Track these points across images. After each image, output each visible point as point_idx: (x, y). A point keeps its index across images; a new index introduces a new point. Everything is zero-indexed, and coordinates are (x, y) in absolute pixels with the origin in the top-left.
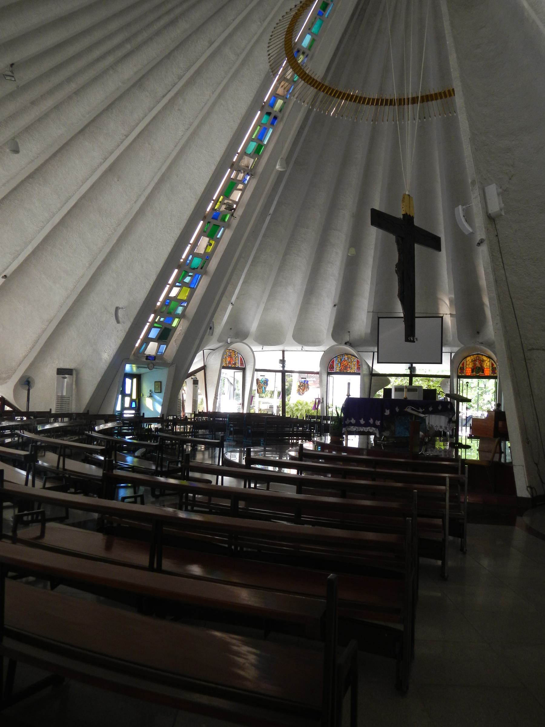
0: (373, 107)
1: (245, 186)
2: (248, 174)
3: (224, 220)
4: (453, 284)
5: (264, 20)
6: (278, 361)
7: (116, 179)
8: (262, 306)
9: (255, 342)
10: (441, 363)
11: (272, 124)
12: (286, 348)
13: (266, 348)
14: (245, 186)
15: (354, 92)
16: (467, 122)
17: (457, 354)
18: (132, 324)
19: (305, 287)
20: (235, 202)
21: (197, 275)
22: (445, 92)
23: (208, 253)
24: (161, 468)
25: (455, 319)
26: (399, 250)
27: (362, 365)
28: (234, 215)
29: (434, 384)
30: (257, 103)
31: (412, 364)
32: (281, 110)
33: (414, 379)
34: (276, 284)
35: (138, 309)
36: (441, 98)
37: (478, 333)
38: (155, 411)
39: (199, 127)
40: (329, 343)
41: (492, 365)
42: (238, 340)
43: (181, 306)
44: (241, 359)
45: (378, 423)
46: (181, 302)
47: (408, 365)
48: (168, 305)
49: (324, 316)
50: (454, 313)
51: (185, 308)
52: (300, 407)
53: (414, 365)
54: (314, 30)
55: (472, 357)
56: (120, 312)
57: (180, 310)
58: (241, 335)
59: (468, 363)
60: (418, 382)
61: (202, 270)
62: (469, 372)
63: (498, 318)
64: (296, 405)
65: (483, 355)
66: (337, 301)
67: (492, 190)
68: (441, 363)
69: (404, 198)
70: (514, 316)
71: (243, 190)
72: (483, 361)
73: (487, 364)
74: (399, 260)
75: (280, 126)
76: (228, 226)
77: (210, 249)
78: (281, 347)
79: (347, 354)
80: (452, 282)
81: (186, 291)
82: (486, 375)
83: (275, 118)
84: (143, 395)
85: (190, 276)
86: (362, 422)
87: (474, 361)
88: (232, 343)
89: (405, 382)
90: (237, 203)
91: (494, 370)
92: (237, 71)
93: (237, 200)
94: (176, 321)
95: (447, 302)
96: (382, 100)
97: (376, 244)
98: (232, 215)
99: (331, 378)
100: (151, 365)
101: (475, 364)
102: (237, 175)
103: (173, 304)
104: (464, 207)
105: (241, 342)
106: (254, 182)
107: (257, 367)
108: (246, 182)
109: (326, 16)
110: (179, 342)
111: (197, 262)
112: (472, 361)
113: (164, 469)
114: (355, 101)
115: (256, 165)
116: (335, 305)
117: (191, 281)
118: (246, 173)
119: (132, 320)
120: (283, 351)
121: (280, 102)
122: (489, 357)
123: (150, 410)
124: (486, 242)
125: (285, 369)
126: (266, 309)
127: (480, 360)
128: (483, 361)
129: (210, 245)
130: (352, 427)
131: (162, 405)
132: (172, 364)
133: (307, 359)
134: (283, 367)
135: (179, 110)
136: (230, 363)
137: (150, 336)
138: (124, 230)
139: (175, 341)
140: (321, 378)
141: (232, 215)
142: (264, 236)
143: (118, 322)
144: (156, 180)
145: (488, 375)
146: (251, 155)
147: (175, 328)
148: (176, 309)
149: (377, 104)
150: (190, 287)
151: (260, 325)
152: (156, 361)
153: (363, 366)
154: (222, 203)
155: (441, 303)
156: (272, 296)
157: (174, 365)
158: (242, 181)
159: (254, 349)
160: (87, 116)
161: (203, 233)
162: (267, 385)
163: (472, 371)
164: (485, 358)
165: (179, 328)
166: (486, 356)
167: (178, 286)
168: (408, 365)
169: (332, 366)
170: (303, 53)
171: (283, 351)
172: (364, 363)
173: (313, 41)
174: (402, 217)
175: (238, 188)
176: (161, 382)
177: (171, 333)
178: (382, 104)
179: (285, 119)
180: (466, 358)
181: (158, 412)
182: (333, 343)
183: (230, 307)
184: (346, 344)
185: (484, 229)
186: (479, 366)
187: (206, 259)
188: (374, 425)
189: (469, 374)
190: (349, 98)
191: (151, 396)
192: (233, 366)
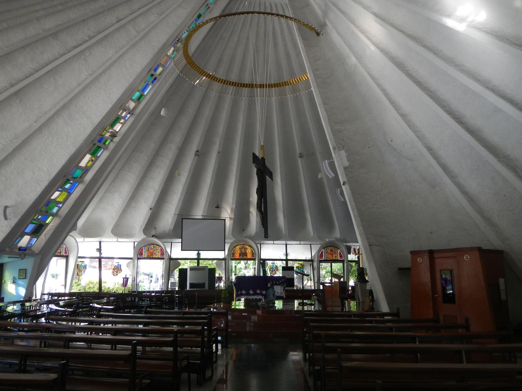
0: (221, 85)
3: (104, 144)
5: (161, 15)
6: (95, 250)
7: (18, 102)
9: (78, 235)
11: (153, 82)
12: (103, 240)
13: (87, 239)
14: (126, 121)
18: (19, 220)
19: (130, 195)
29: (212, 265)
32: (160, 75)
33: (200, 261)
35: (27, 208)
38: (18, 295)
39: (101, 74)
40: (140, 237)
41: (252, 251)
43: (57, 206)
44: (65, 249)
45: (264, 292)
49: (140, 215)
52: (92, 286)
53: (200, 252)
56: (8, 210)
57: (55, 210)
60: (203, 264)
63: (361, 227)
64: (88, 284)
66: (153, 206)
71: (123, 124)
72: (247, 249)
73: (249, 251)
75: (157, 84)
78: (98, 239)
79: (153, 244)
81: (65, 194)
83: (155, 79)
84: (5, 282)
85: (70, 183)
86: (251, 292)
87: (241, 249)
89: (194, 264)
91: (253, 254)
92: (137, 43)
93: (117, 130)
96: (228, 81)
97: (190, 170)
98: (112, 140)
99: (141, 261)
100: (23, 255)
101: (241, 251)
102: (122, 113)
103: (52, 204)
106: (132, 119)
107: (79, 255)
108: (127, 118)
110: (48, 236)
114: (219, 82)
115: (135, 108)
116: (151, 209)
119: (19, 217)
120: (100, 242)
121: (160, 69)
122: (250, 246)
123: (13, 295)
125: (102, 256)
128: (247, 249)
131: (26, 290)
133: (125, 248)
134: (101, 254)
137: (26, 231)
138: (21, 143)
139: (45, 235)
140: (134, 262)
141: (112, 140)
143: (6, 218)
144: (58, 108)
147: (48, 224)
149: (224, 83)
152: (27, 252)
158: (124, 118)
160: (6, 49)
162: (86, 268)
163: (240, 255)
164: (248, 247)
165: (50, 225)
167: (59, 191)
168: (197, 252)
169: (142, 253)
176: (26, 270)
178: (227, 84)
181: (21, 296)
182: (143, 236)
184: (153, 236)
188: (261, 294)
190: (208, 76)
191: (14, 282)
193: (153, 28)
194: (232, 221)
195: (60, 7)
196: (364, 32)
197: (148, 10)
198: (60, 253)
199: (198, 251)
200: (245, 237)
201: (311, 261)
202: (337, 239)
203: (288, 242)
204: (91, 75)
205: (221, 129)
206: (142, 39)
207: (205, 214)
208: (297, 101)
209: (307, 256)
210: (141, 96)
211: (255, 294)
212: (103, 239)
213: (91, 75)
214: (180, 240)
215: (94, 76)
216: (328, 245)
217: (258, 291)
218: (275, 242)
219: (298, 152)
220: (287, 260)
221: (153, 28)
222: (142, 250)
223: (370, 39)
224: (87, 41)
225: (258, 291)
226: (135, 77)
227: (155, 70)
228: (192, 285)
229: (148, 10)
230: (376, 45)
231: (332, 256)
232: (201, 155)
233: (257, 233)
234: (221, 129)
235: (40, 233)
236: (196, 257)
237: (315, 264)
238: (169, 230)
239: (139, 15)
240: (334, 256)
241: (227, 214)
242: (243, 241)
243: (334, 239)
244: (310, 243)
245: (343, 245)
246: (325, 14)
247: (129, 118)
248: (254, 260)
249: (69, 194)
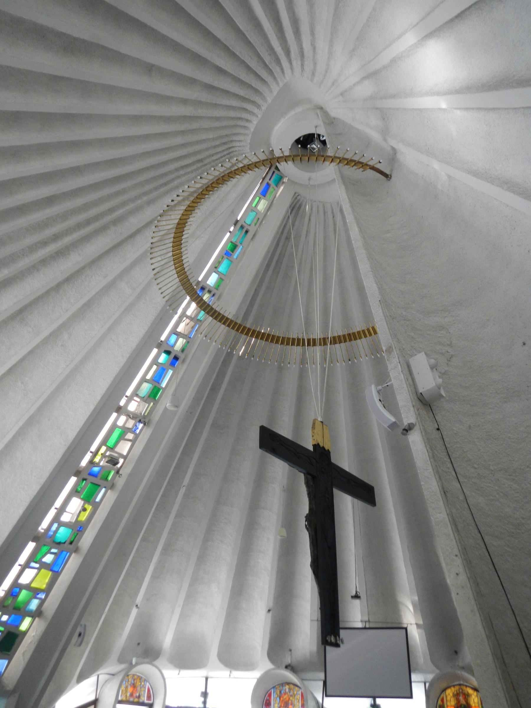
1: (137, 436)
2: (140, 421)
4: (414, 582)
6: (200, 694)
8: (178, 612)
10: (411, 697)
11: (172, 364)
14: (137, 436)
16: (375, 285)
17: (432, 684)
20: (122, 456)
21: (64, 553)
22: (368, 330)
23: (81, 521)
25: (422, 631)
26: (309, 494)
27: (307, 700)
28: (120, 472)
30: (151, 339)
31: (374, 698)
32: (183, 350)
34: (195, 580)
36: (366, 336)
37: (456, 652)
39: (82, 362)
40: (265, 666)
42: (146, 660)
43: (36, 598)
44: (149, 690)
46: (35, 592)
48: (16, 596)
49: (257, 627)
50: (421, 622)
51: (43, 602)
53: (379, 701)
54: (222, 268)
57: (34, 605)
58: (150, 653)
59: (449, 698)
61: (71, 546)
65: (466, 686)
66: (271, 605)
67: (420, 363)
68: (411, 697)
69: (314, 424)
70: (491, 567)
71: (133, 441)
74: (310, 509)
75: (181, 367)
76: (112, 486)
77: (84, 517)
78: (201, 673)
79: (288, 684)
80: (412, 577)
81: (46, 576)
83: (176, 358)
87: (456, 696)
88: (137, 664)
90: (125, 458)
94: (27, 621)
95: (411, 607)
101: (458, 701)
103: (23, 595)
104: (380, 387)
105: (150, 663)
106: (148, 432)
108: (138, 431)
109: (235, 257)
111: (63, 534)
112: (454, 695)
116: (269, 611)
117: (55, 562)
118: (138, 419)
120: (207, 679)
124: (417, 428)
126: (183, 616)
129: (84, 510)
132: (14, 691)
136: (131, 695)
139: (23, 654)
142: (179, 515)
144: (21, 424)
146: (145, 399)
147: (25, 633)
148: (28, 602)
150: (51, 570)
151: (176, 639)
153: (309, 702)
154: (103, 455)
155: (402, 608)
156: (191, 597)
157: (17, 695)
159: (166, 672)
161: (75, 492)
164: (470, 691)
170: (209, 292)
171: (207, 679)
172: (309, 697)
173: (221, 279)
174: (311, 448)
175: (127, 437)
177: (17, 641)
179: (188, 361)
180: (444, 690)
182: (268, 665)
183: (134, 612)
184: (286, 667)
185: (412, 408)
187: (78, 531)
192: (136, 700)
198: (139, 697)
199: (374, 698)
200: (463, 668)
203: (211, 674)
207: (366, 619)
212: (211, 674)
214: (322, 675)
222: (270, 696)
226: (128, 355)
235: (13, 650)
242: (459, 678)
247: (141, 431)
249: (56, 575)
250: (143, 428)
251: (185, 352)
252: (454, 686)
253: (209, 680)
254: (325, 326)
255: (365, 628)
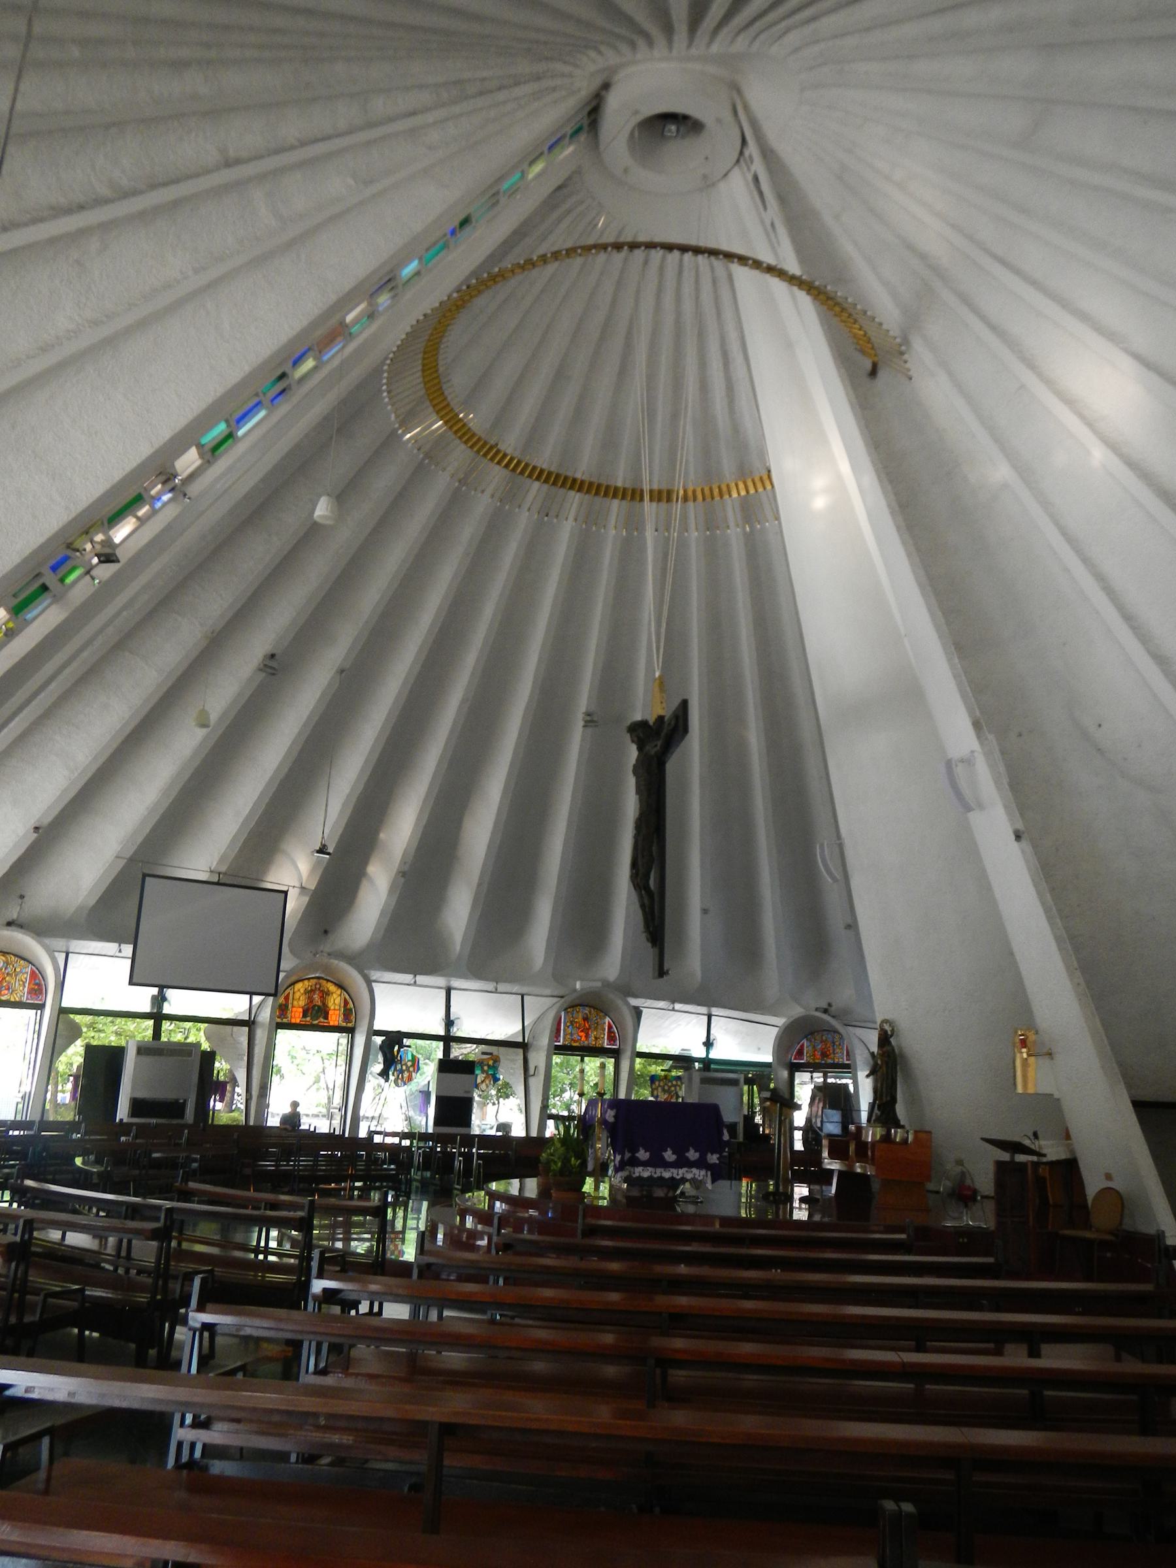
10: (131, 983)
14: (154, 512)
15: (467, 415)
24: (20, 1318)
29: (198, 1036)
31: (162, 988)
33: (166, 1025)
37: (326, 932)
39: (128, 332)
41: (346, 1003)
45: (713, 1159)
47: (155, 991)
55: (306, 982)
59: (297, 995)
60: (172, 1033)
62: (296, 1016)
63: (1078, 973)
68: (131, 983)
71: (142, 521)
72: (328, 993)
73: (335, 1001)
75: (284, 408)
82: (332, 1024)
86: (669, 1156)
87: (309, 993)
91: (347, 1014)
101: (311, 1000)
108: (158, 505)
112: (306, 992)
113: (28, 1319)
116: (36, 829)
121: (309, 364)
122: (340, 986)
123: (1083, 1195)
127: (322, 991)
128: (328, 993)
130: (640, 1169)
135: (78, 262)
145: (336, 1024)
163: (305, 1015)
164: (332, 988)
166: (336, 984)
171: (710, 1017)
180: (294, 983)
186: (319, 1003)
188: (701, 1164)
189: (298, 1021)
193: (333, 219)
194: (306, 899)
195: (76, 52)
196: (1070, 402)
197: (329, 156)
201: (523, 1046)
202: (606, 984)
203: (456, 983)
204: (96, 323)
205: (370, 597)
206: (290, 245)
208: (714, 551)
209: (504, 1027)
210: (230, 436)
211: (657, 1161)
213: (96, 323)
214: (128, 949)
215: (106, 331)
216: (578, 1002)
217: (692, 1155)
218: (420, 979)
219: (583, 709)
220: (448, 1040)
221: (333, 219)
223: (1090, 425)
224: (106, 201)
225: (692, 1155)
227: (297, 362)
228: (138, 1107)
229: (329, 156)
230: (1113, 446)
231: (587, 1036)
232: (277, 669)
233: (370, 946)
234: (370, 597)
236: (146, 1008)
237: (538, 1059)
238: (80, 908)
239: (301, 165)
240: (593, 1034)
241: (294, 872)
242: (327, 968)
243: (599, 984)
244: (524, 990)
245: (628, 1004)
246: (913, 320)
248: (351, 1031)
250: (170, 500)
251: (279, 373)
252: (309, 979)
253: (453, 992)
254: (535, 435)
255: (218, 884)
